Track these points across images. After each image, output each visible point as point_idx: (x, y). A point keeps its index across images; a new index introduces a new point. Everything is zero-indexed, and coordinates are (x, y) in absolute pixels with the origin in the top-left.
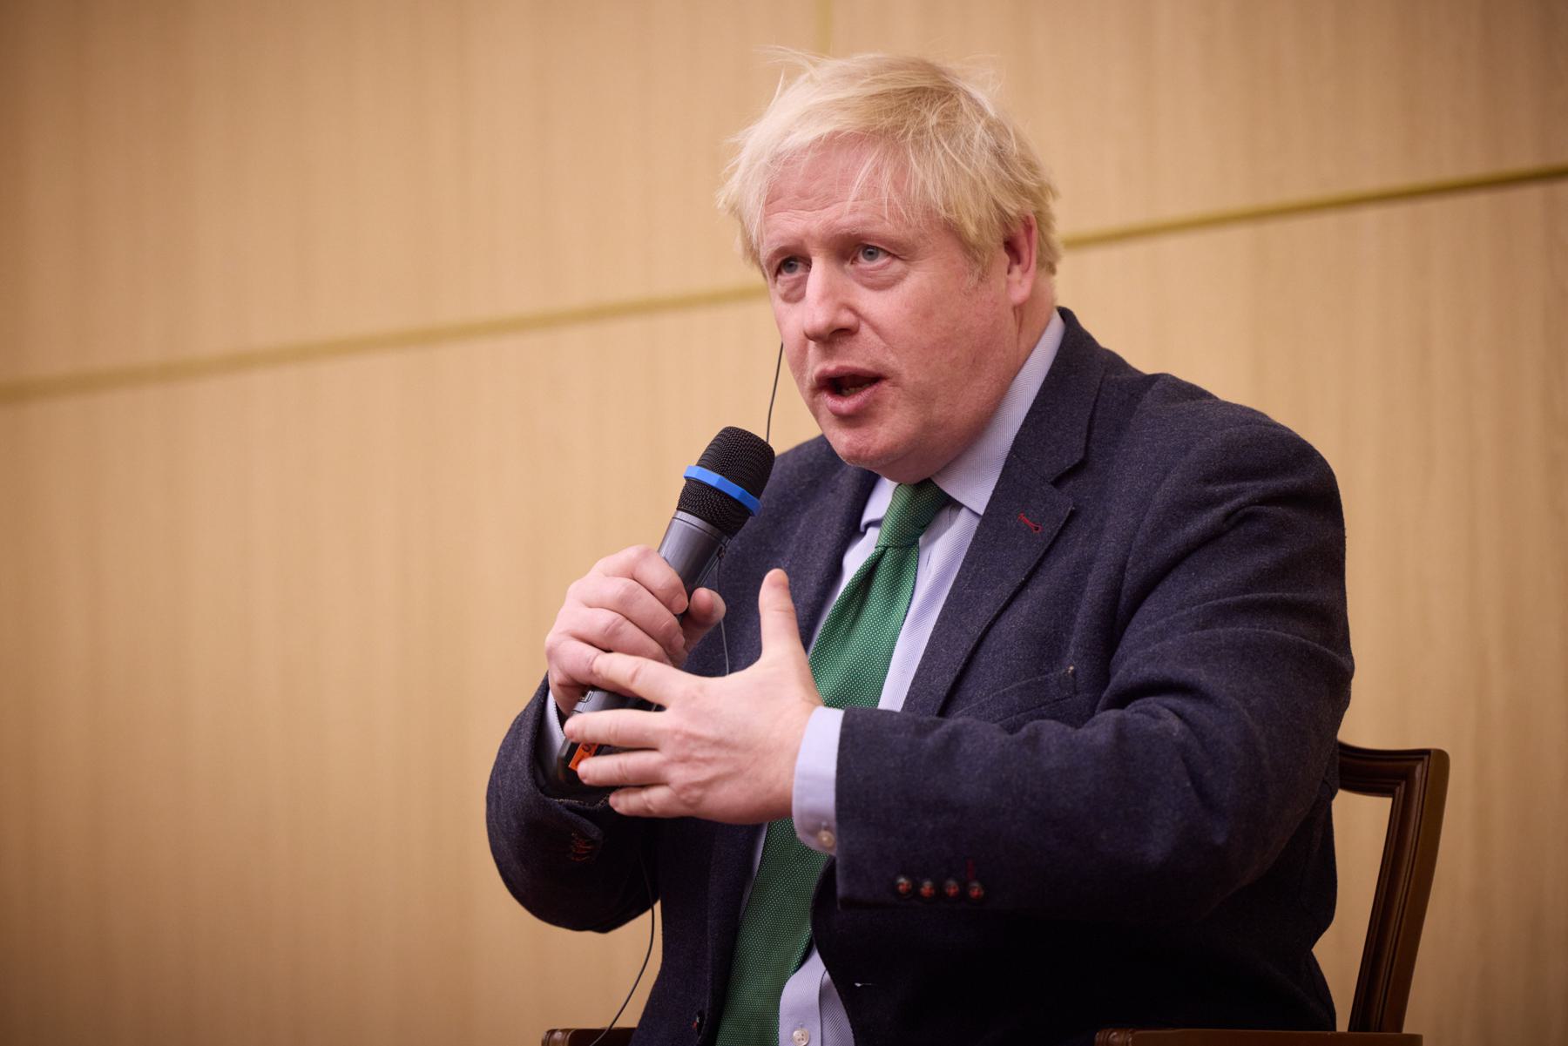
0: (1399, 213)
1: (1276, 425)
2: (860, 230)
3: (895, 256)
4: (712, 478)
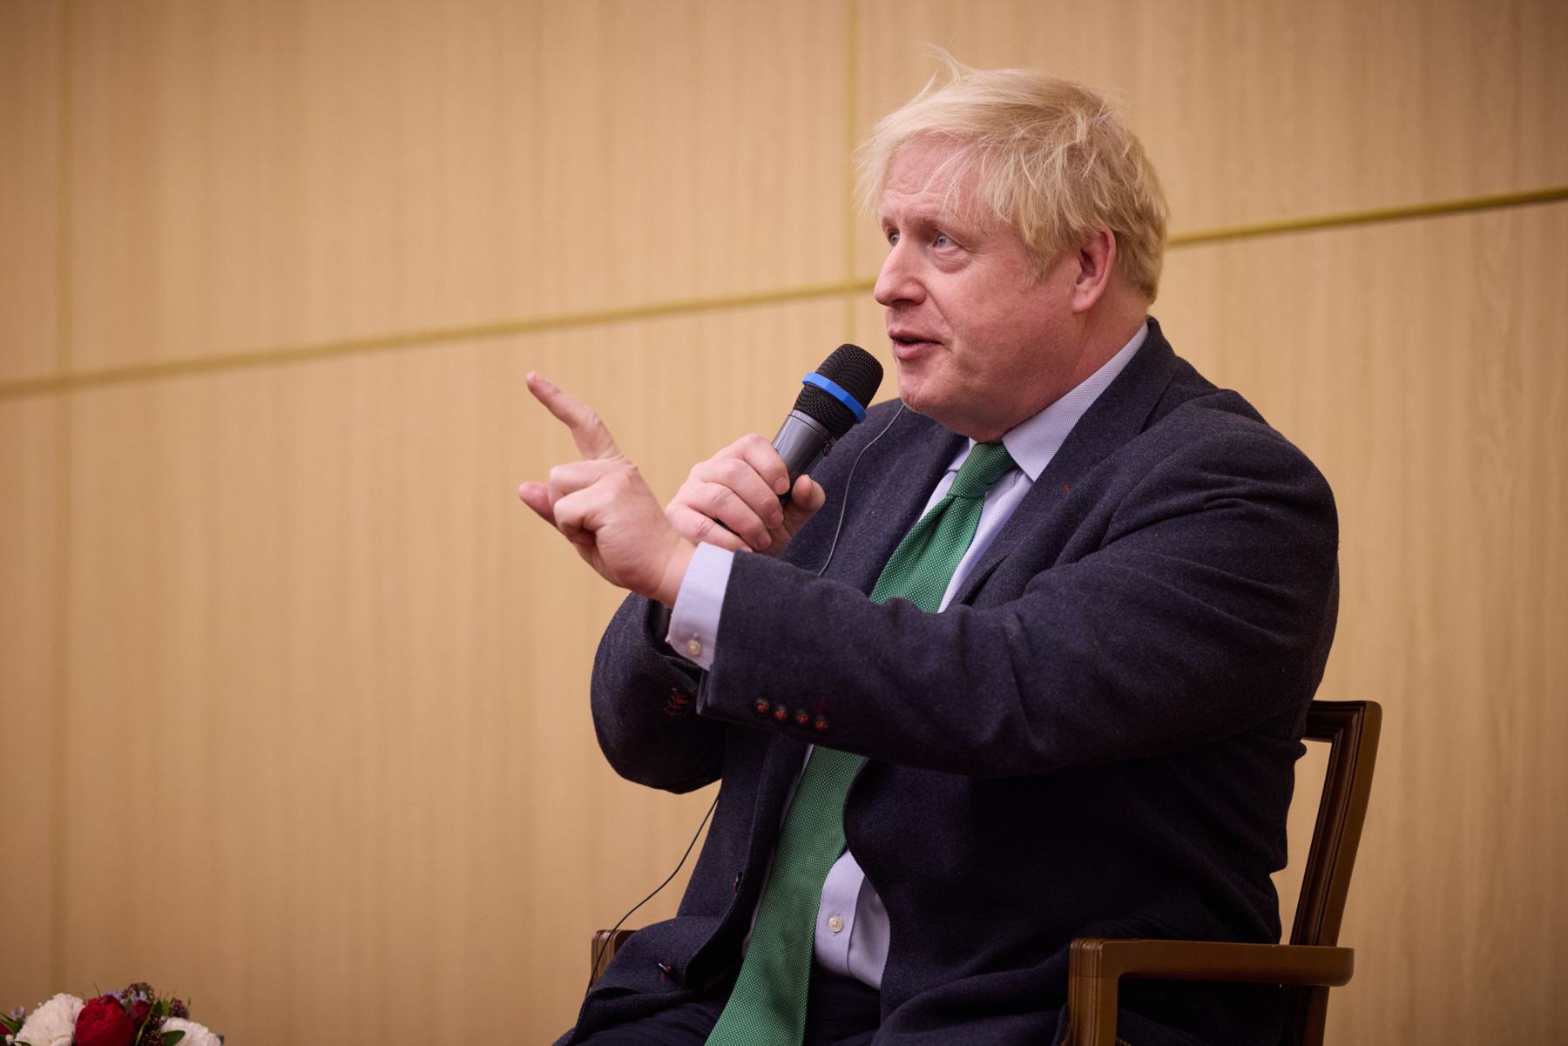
0: (1348, 235)
1: (1277, 436)
2: (930, 217)
3: (961, 247)
4: (824, 383)
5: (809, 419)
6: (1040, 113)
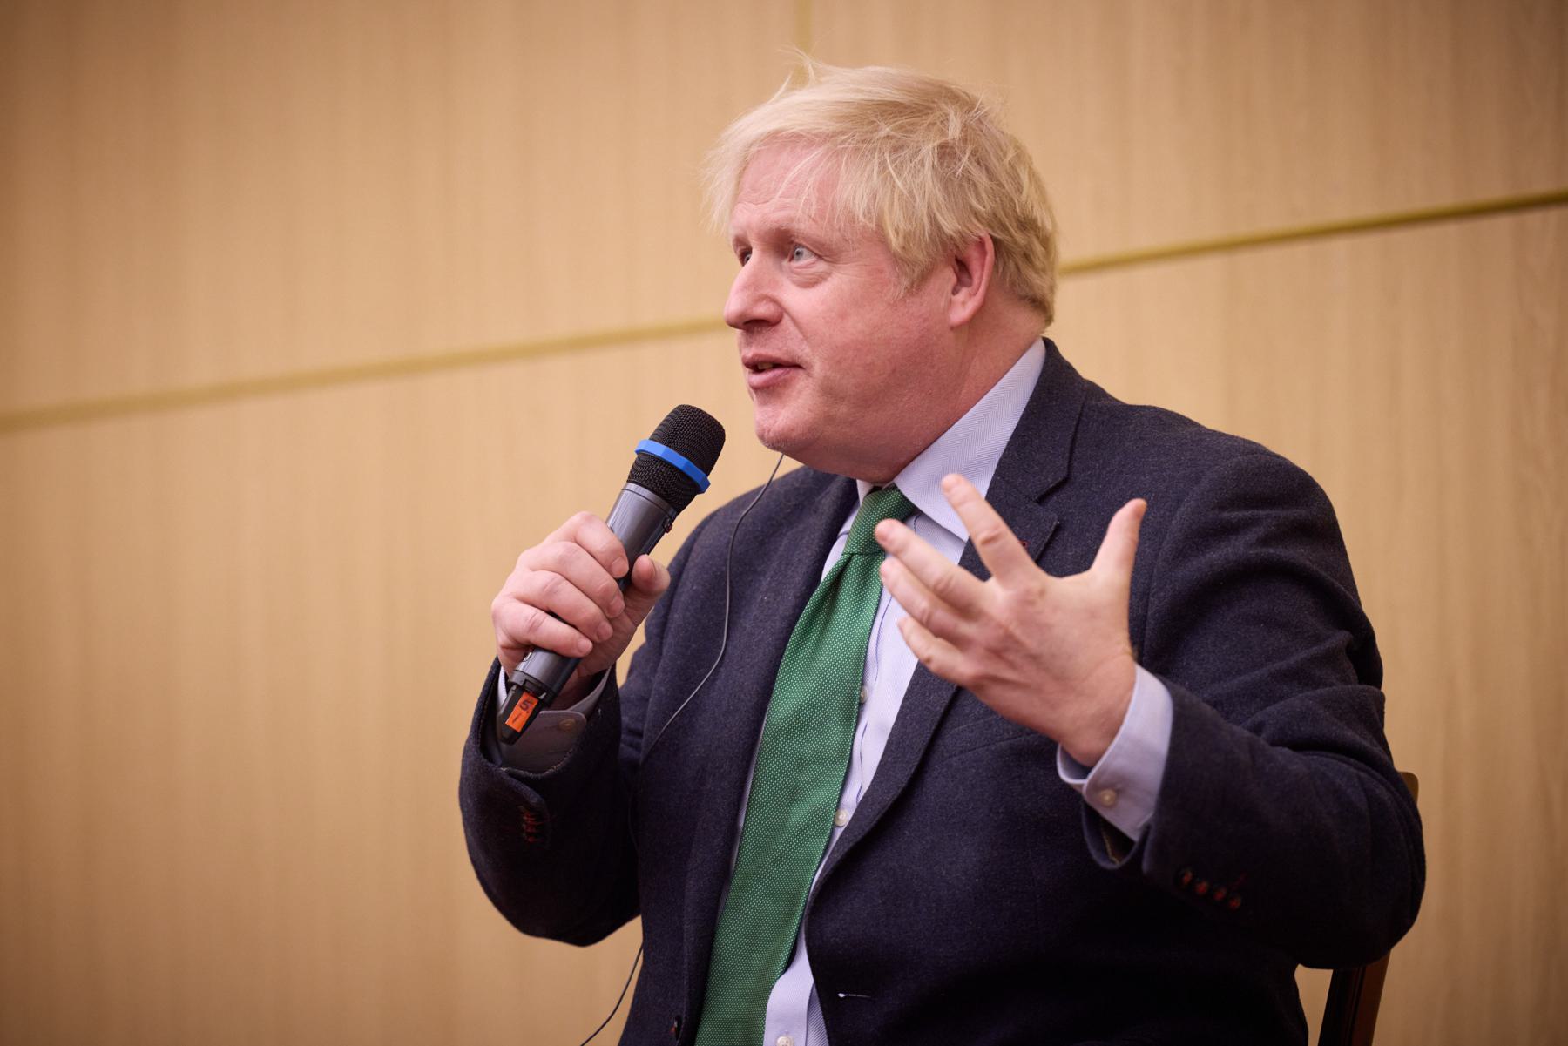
3: (820, 257)
4: (659, 450)
5: (646, 493)
6: (908, 112)
